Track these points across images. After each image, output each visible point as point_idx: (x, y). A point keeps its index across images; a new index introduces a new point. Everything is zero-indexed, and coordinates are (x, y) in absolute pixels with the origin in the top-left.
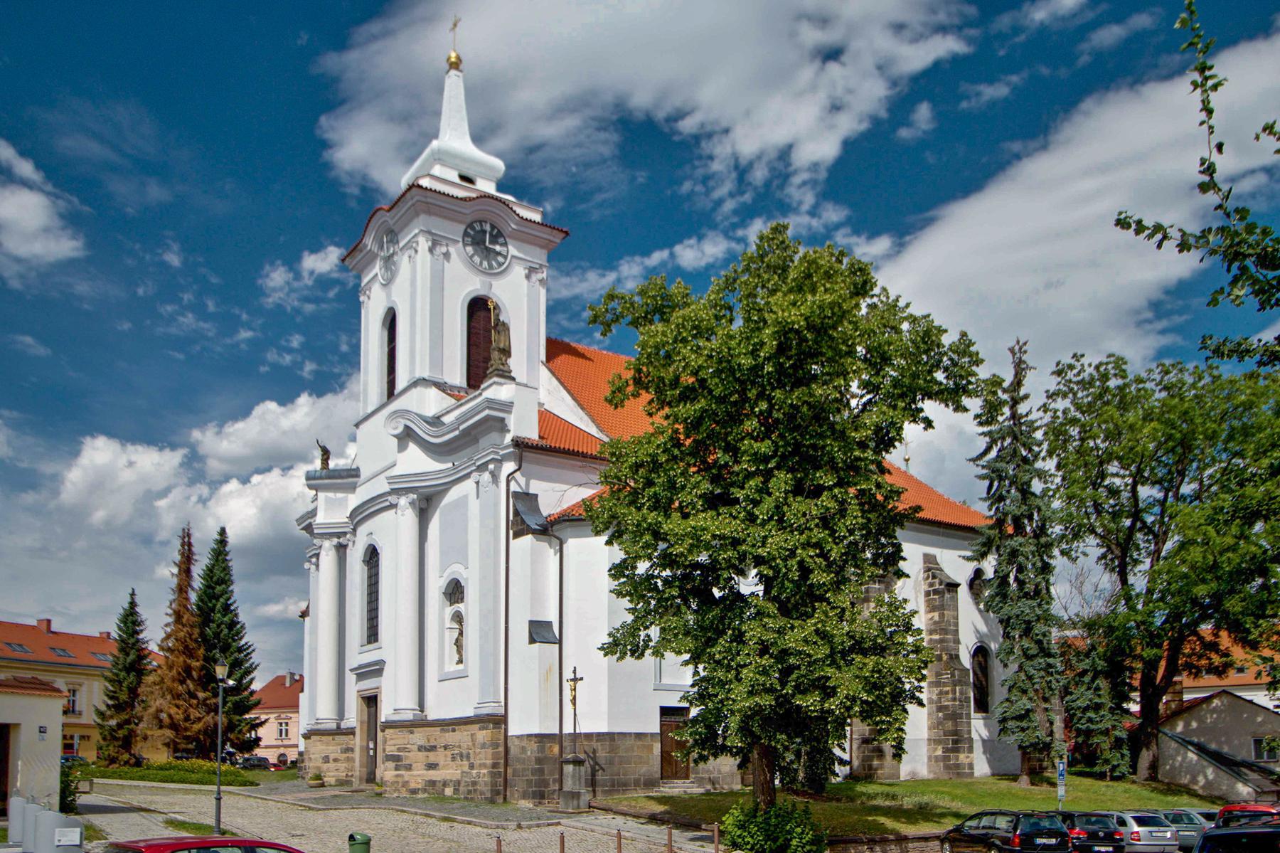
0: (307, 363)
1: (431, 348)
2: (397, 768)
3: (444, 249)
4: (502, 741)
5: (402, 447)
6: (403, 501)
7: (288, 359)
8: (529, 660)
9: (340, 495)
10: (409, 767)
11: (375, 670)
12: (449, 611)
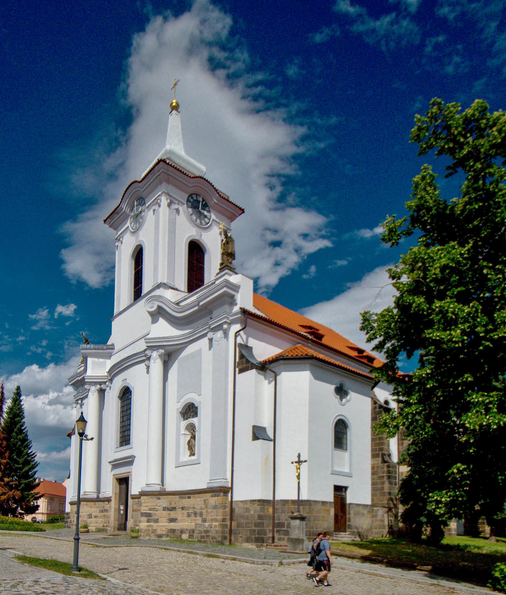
0: (48, 352)
1: (168, 264)
2: (148, 521)
3: (176, 206)
4: (228, 505)
5: (154, 321)
6: (155, 354)
7: (40, 350)
8: (250, 451)
9: (101, 360)
10: (157, 521)
11: (129, 461)
12: (184, 424)
